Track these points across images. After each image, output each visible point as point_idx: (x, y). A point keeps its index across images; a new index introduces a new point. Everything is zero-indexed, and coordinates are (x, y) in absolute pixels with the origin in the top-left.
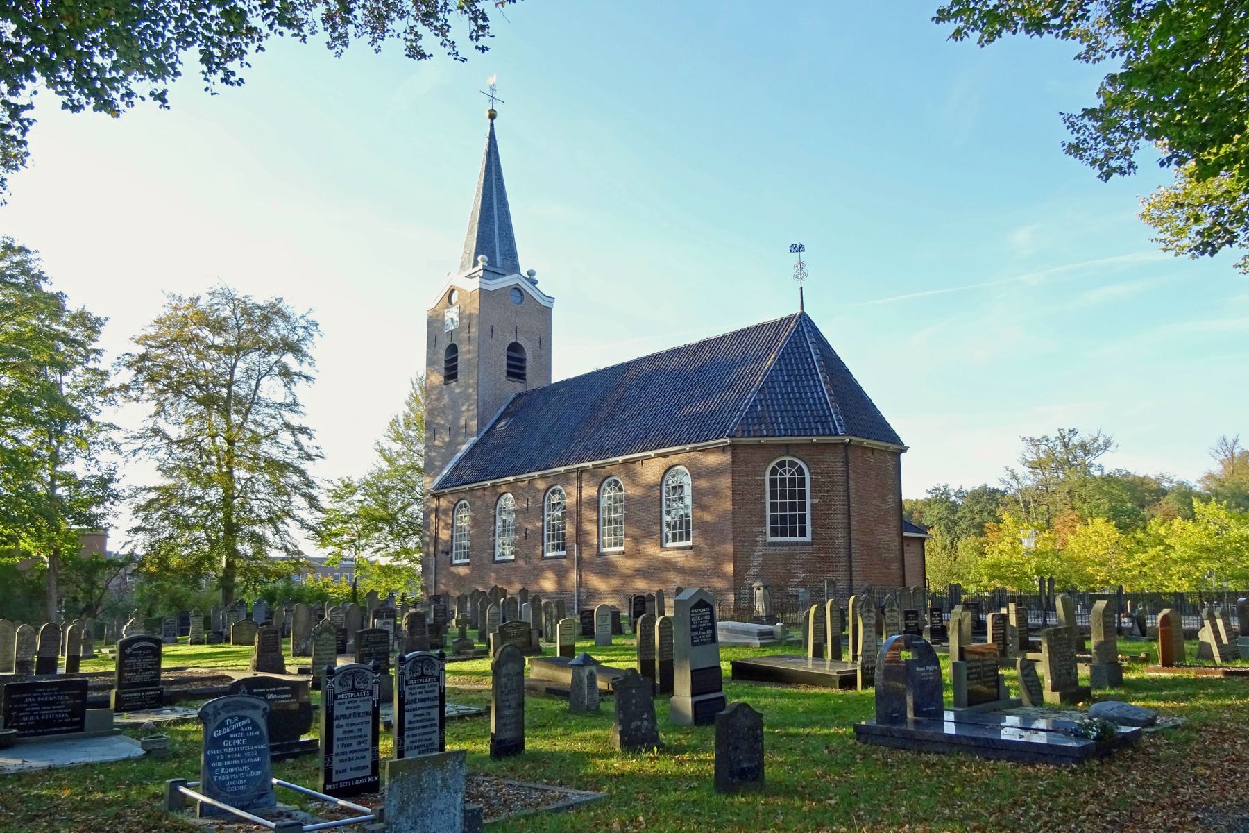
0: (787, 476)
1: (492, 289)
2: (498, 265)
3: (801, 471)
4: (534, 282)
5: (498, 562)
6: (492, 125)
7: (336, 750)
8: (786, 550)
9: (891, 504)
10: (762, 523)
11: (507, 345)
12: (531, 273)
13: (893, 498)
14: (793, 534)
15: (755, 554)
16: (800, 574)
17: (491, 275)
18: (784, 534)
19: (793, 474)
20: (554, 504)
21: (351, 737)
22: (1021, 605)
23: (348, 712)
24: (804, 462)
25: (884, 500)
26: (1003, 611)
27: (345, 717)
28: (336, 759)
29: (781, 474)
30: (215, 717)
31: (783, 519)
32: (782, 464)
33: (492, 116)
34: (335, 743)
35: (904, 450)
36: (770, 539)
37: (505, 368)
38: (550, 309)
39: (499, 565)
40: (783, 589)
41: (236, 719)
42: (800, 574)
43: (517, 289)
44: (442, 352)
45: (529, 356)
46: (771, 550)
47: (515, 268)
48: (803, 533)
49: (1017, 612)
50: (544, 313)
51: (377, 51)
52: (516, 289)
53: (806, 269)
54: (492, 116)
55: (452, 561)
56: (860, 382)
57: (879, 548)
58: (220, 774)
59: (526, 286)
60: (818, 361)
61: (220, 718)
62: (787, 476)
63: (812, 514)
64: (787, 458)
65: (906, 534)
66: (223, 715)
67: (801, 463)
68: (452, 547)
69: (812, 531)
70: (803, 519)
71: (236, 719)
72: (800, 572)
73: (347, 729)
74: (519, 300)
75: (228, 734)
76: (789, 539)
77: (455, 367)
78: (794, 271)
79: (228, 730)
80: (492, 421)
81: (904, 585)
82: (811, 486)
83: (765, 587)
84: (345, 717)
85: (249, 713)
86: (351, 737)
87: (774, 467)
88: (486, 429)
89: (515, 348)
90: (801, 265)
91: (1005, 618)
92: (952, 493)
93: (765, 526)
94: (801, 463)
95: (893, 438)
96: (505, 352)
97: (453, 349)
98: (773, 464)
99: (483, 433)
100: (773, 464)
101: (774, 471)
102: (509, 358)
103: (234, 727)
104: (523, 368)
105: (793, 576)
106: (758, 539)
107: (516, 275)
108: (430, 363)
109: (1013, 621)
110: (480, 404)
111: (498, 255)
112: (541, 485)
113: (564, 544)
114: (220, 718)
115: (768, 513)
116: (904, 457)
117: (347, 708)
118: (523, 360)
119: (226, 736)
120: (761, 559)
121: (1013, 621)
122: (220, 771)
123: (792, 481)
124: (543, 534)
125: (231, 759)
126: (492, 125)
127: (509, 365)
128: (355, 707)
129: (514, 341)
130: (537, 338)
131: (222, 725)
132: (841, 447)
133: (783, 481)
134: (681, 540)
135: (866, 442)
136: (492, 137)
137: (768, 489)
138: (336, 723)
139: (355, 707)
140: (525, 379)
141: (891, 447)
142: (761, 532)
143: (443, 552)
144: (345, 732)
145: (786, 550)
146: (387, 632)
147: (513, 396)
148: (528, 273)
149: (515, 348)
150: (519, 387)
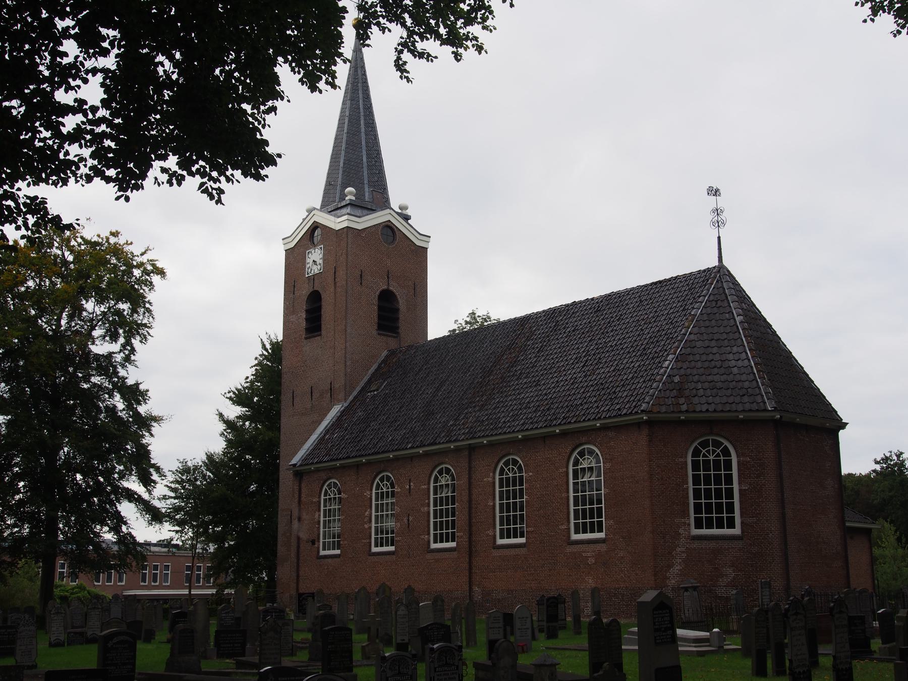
0: (711, 458)
2: (367, 198)
3: (726, 452)
4: (407, 218)
8: (713, 545)
11: (378, 293)
14: (720, 526)
15: (678, 549)
16: (730, 573)
17: (358, 212)
18: (709, 526)
19: (718, 455)
20: (441, 486)
24: (731, 442)
29: (704, 456)
31: (709, 507)
35: (843, 426)
36: (696, 532)
38: (425, 250)
39: (375, 558)
42: (730, 573)
44: (302, 307)
45: (402, 304)
46: (696, 544)
47: (383, 202)
48: (731, 525)
50: (419, 255)
51: (495, 29)
52: (388, 226)
53: (723, 216)
55: (318, 552)
56: (790, 347)
59: (399, 223)
62: (711, 458)
63: (741, 502)
64: (710, 438)
65: (848, 524)
67: (726, 443)
68: (319, 535)
69: (742, 523)
72: (730, 571)
76: (715, 531)
77: (319, 318)
78: (711, 217)
81: (849, 587)
82: (739, 470)
87: (696, 446)
88: (355, 393)
90: (717, 211)
93: (689, 515)
94: (726, 443)
97: (315, 299)
99: (351, 398)
101: (696, 453)
106: (681, 531)
107: (388, 211)
111: (366, 186)
112: (167, 94)
113: (453, 533)
118: (397, 310)
120: (684, 555)
123: (717, 464)
124: (429, 521)
127: (380, 317)
129: (385, 287)
133: (707, 463)
134: (592, 531)
137: (690, 473)
140: (398, 333)
142: (685, 523)
145: (713, 545)
147: (385, 353)
148: (400, 208)
150: (393, 343)
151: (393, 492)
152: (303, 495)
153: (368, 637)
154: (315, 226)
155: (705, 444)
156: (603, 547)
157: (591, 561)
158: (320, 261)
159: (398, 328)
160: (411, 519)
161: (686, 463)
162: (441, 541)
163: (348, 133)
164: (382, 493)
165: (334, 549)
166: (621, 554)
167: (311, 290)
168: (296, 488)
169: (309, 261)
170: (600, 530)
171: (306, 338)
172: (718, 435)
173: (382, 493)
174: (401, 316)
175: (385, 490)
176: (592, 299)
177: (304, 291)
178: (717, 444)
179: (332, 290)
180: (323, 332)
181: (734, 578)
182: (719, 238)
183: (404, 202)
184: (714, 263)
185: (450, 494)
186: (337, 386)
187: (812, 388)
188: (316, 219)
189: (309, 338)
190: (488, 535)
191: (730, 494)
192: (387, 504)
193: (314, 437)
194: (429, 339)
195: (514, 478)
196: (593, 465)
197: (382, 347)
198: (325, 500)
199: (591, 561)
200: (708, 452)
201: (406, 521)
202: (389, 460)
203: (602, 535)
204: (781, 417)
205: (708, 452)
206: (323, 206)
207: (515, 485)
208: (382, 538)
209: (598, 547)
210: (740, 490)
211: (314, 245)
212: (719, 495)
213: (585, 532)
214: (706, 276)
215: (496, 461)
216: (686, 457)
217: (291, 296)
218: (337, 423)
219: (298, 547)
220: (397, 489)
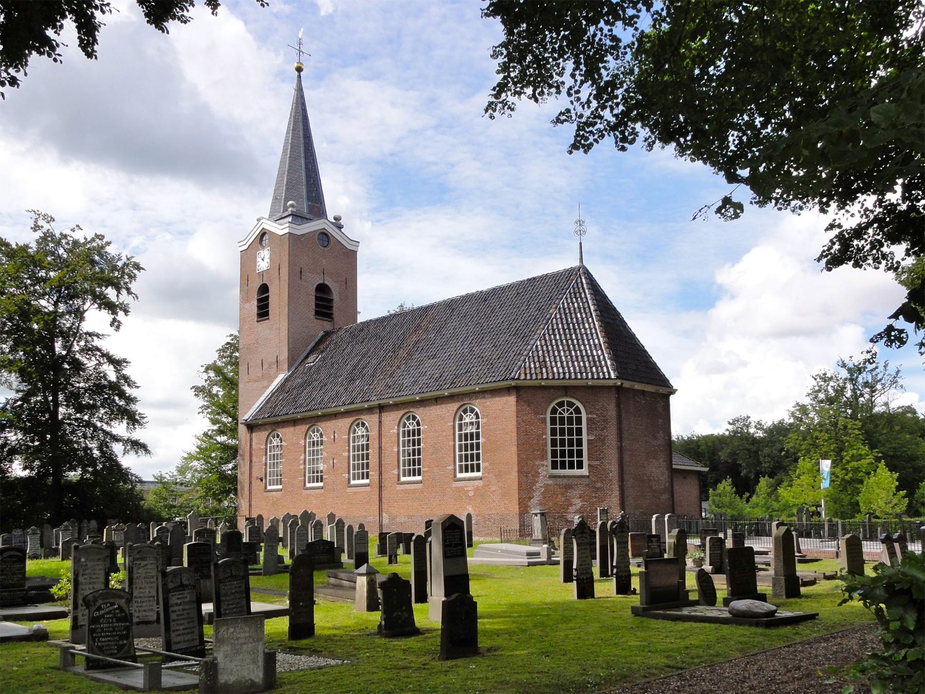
0: (566, 415)
1: (299, 233)
3: (578, 411)
4: (340, 227)
5: (352, 486)
6: (299, 77)
7: (172, 628)
8: (565, 481)
9: (661, 441)
10: (543, 457)
11: (315, 287)
12: (337, 219)
13: (662, 435)
14: (571, 467)
15: (538, 485)
18: (563, 467)
19: (571, 413)
21: (183, 619)
22: (736, 531)
23: (179, 601)
25: (655, 438)
26: (721, 535)
27: (177, 605)
28: (173, 635)
29: (560, 413)
30: (95, 603)
32: (561, 404)
33: (299, 70)
34: (172, 624)
35: (673, 392)
37: (314, 307)
40: (562, 516)
41: (109, 605)
43: (324, 235)
45: (335, 296)
48: (580, 466)
49: (734, 536)
50: (351, 256)
54: (299, 70)
57: (650, 480)
58: (99, 641)
59: (332, 231)
60: (595, 310)
61: (98, 604)
62: (566, 415)
63: (589, 449)
65: (674, 467)
66: (100, 602)
67: (578, 404)
69: (589, 465)
70: (580, 454)
71: (109, 605)
73: (178, 613)
74: (326, 243)
75: (103, 615)
77: (267, 306)
79: (103, 612)
80: (302, 357)
82: (588, 424)
83: (542, 514)
84: (177, 605)
85: (117, 601)
86: (183, 619)
87: (554, 407)
89: (322, 289)
91: (722, 542)
92: (753, 424)
94: (578, 404)
95: (663, 382)
96: (313, 292)
97: (264, 289)
98: (554, 404)
100: (554, 404)
101: (554, 411)
102: (317, 298)
103: (107, 610)
104: (331, 308)
105: (571, 505)
107: (324, 220)
108: (244, 299)
109: (729, 544)
110: (291, 340)
113: (368, 473)
114: (98, 604)
115: (549, 448)
116: (672, 398)
117: (178, 599)
118: (331, 301)
119: (103, 616)
121: (729, 544)
122: (99, 640)
123: (570, 420)
125: (106, 632)
126: (299, 77)
127: (317, 305)
128: (184, 598)
129: (321, 282)
130: (343, 279)
131: (99, 609)
132: (614, 391)
135: (638, 386)
136: (300, 90)
138: (171, 609)
139: (184, 598)
140: (332, 318)
141: (662, 390)
143: (257, 478)
144: (178, 615)
145: (565, 481)
146: (210, 545)
147: (321, 333)
148: (335, 219)
149: (322, 289)
150: (327, 326)
151: (322, 441)
152: (254, 444)
153: (735, 484)
154: (263, 234)
155: (561, 404)
156: (479, 483)
157: (471, 494)
158: (259, 259)
159: (332, 314)
160: (335, 461)
161: (545, 419)
162: (358, 479)
163: (290, 157)
164: (314, 442)
165: (277, 485)
166: (493, 488)
167: (261, 283)
168: (248, 438)
169: (267, 260)
170: (478, 470)
171: (258, 322)
172: (571, 397)
173: (314, 442)
174: (335, 305)
175: (315, 439)
176: (481, 292)
177: (257, 285)
178: (571, 404)
179: (277, 283)
180: (270, 316)
181: (581, 507)
182: (581, 243)
183: (337, 214)
184: (576, 263)
185: (365, 443)
186: (281, 359)
187: (651, 362)
188: (264, 226)
189: (260, 321)
190: (393, 474)
191: (580, 443)
192: (277, 455)
193: (262, 399)
194: (361, 319)
195: (414, 430)
196: (474, 420)
197: (320, 327)
198: (270, 447)
199: (471, 494)
200: (564, 410)
201: (331, 463)
202: (319, 417)
203: (479, 474)
204: (622, 384)
205: (564, 410)
206: (270, 216)
207: (414, 435)
208: (273, 479)
209: (477, 483)
210: (588, 440)
211: (263, 248)
212: (571, 443)
213: (467, 471)
214: (570, 274)
215: (400, 417)
216: (545, 414)
217: (246, 287)
218: (282, 388)
219: (250, 483)
220: (325, 439)
